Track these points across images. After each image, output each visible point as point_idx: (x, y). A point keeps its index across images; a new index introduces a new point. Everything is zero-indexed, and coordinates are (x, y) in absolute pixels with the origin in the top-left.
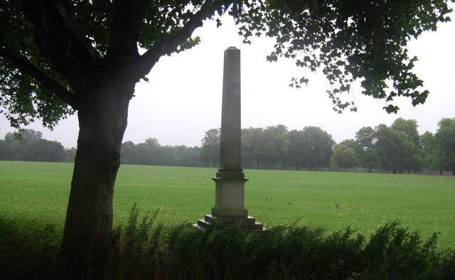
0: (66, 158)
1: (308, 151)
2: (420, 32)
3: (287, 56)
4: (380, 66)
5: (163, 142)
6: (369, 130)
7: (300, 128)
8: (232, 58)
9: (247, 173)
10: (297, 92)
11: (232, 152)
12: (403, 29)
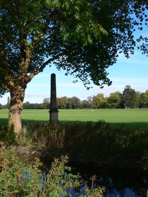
0: (47, 173)
1: (73, 104)
2: (108, 66)
3: (71, 74)
4: (99, 76)
5: (31, 103)
6: (90, 97)
7: (71, 97)
8: (53, 77)
9: (59, 110)
10: (73, 86)
11: (54, 104)
12: (103, 67)
